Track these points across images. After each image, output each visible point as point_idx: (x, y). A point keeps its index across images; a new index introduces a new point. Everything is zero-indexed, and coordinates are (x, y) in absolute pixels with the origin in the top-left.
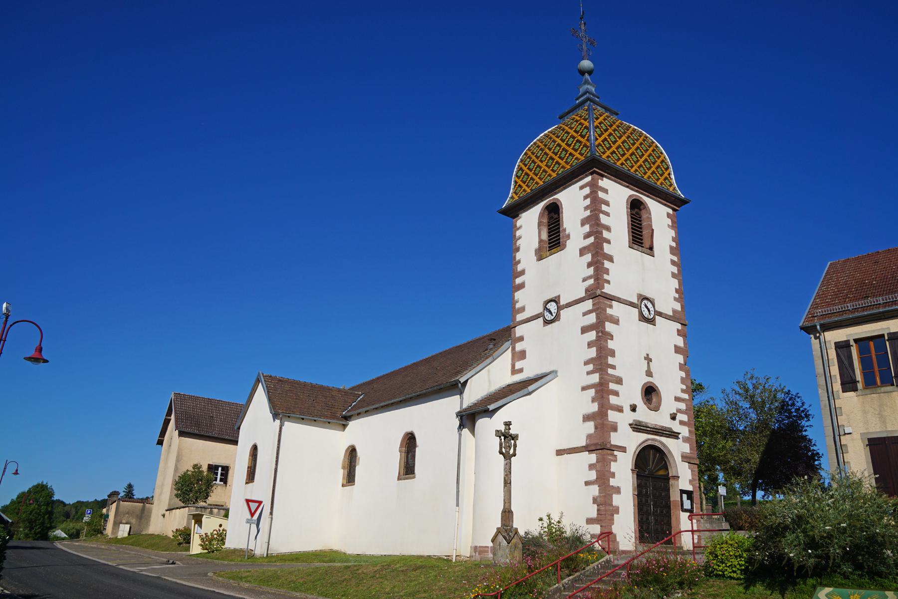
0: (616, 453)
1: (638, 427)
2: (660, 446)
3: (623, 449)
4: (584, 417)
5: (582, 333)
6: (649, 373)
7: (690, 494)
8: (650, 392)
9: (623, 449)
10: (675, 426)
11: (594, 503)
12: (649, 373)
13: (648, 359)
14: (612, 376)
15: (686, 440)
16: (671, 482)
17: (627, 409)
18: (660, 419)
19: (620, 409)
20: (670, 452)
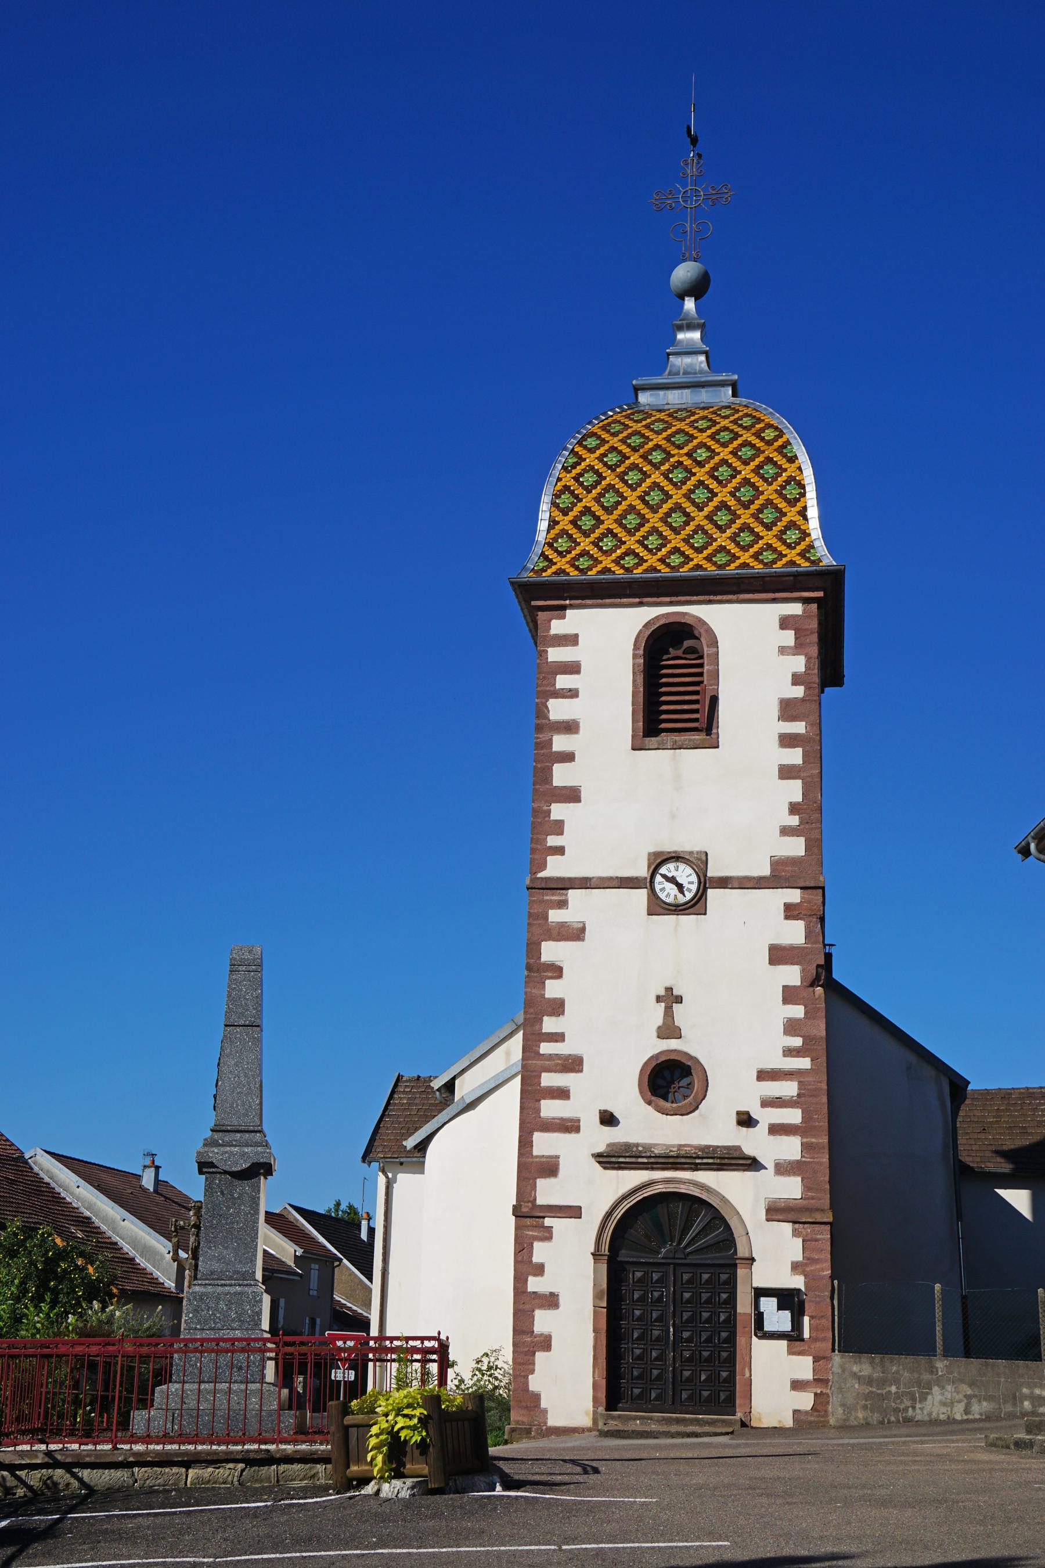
0: (548, 1222)
1: (612, 1159)
2: (696, 1192)
3: (574, 1212)
4: (563, 1040)
5: (576, 636)
6: (669, 1030)
7: (787, 1299)
8: (671, 1080)
9: (574, 1212)
10: (754, 1142)
11: (201, 1172)
12: (669, 1030)
13: (670, 998)
14: (550, 1057)
15: (783, 1169)
16: (741, 1272)
17: (590, 1121)
18: (709, 1126)
19: (570, 1126)
20: (724, 1200)
